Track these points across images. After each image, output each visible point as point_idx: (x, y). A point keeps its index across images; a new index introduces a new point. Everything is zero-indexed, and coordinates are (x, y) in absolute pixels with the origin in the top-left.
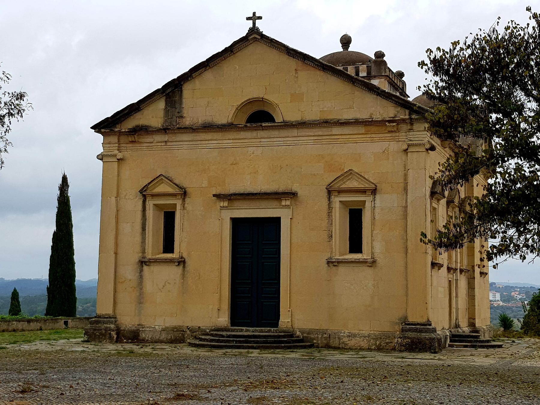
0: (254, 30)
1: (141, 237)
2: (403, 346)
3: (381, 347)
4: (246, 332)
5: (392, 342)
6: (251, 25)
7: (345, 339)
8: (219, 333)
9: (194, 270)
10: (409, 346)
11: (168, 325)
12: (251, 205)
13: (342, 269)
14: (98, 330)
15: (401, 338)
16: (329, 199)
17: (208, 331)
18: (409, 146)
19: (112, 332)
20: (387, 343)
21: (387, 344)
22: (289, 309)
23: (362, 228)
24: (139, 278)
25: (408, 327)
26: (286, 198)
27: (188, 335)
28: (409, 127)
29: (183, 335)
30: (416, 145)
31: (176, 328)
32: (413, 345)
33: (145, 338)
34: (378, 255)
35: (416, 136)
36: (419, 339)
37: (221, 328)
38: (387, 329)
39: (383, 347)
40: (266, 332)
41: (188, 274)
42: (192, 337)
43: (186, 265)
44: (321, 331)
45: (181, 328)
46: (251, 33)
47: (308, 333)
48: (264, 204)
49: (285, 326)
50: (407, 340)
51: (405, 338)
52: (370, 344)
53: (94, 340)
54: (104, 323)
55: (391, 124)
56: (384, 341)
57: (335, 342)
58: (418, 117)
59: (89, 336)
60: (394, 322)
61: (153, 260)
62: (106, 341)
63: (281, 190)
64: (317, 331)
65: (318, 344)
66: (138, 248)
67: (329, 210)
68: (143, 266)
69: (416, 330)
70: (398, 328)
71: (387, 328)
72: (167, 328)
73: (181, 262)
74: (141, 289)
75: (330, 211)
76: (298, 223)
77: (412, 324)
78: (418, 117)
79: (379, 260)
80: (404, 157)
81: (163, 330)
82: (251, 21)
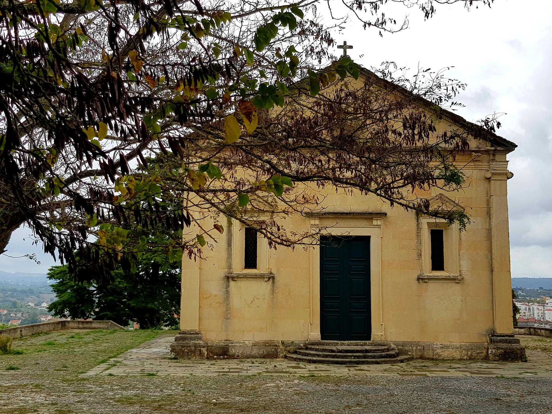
0: (345, 58)
1: (227, 253)
2: (497, 356)
3: (473, 357)
4: (341, 345)
5: (482, 353)
6: (342, 54)
7: (439, 351)
11: (257, 340)
13: (432, 285)
14: (187, 347)
15: (494, 349)
16: (418, 219)
17: (302, 345)
18: (493, 174)
19: (202, 349)
20: (478, 354)
21: (478, 355)
22: (381, 324)
23: (256, 257)
24: (226, 294)
25: (499, 338)
26: (378, 219)
27: (281, 349)
28: (491, 158)
29: (276, 350)
30: (499, 174)
31: (268, 343)
35: (498, 166)
38: (475, 340)
39: (474, 357)
40: (362, 345)
43: (276, 281)
44: (414, 343)
45: (273, 343)
47: (402, 346)
48: (353, 223)
50: (501, 351)
51: (498, 348)
53: (182, 357)
54: (191, 339)
57: (429, 354)
58: (502, 149)
60: (481, 334)
62: (196, 358)
63: (370, 211)
64: (411, 344)
66: (224, 264)
68: (229, 282)
69: (506, 341)
71: (475, 339)
72: (258, 342)
73: (271, 278)
74: (228, 305)
77: (501, 336)
78: (502, 149)
79: (466, 277)
80: (486, 184)
81: (254, 345)
82: (347, 50)
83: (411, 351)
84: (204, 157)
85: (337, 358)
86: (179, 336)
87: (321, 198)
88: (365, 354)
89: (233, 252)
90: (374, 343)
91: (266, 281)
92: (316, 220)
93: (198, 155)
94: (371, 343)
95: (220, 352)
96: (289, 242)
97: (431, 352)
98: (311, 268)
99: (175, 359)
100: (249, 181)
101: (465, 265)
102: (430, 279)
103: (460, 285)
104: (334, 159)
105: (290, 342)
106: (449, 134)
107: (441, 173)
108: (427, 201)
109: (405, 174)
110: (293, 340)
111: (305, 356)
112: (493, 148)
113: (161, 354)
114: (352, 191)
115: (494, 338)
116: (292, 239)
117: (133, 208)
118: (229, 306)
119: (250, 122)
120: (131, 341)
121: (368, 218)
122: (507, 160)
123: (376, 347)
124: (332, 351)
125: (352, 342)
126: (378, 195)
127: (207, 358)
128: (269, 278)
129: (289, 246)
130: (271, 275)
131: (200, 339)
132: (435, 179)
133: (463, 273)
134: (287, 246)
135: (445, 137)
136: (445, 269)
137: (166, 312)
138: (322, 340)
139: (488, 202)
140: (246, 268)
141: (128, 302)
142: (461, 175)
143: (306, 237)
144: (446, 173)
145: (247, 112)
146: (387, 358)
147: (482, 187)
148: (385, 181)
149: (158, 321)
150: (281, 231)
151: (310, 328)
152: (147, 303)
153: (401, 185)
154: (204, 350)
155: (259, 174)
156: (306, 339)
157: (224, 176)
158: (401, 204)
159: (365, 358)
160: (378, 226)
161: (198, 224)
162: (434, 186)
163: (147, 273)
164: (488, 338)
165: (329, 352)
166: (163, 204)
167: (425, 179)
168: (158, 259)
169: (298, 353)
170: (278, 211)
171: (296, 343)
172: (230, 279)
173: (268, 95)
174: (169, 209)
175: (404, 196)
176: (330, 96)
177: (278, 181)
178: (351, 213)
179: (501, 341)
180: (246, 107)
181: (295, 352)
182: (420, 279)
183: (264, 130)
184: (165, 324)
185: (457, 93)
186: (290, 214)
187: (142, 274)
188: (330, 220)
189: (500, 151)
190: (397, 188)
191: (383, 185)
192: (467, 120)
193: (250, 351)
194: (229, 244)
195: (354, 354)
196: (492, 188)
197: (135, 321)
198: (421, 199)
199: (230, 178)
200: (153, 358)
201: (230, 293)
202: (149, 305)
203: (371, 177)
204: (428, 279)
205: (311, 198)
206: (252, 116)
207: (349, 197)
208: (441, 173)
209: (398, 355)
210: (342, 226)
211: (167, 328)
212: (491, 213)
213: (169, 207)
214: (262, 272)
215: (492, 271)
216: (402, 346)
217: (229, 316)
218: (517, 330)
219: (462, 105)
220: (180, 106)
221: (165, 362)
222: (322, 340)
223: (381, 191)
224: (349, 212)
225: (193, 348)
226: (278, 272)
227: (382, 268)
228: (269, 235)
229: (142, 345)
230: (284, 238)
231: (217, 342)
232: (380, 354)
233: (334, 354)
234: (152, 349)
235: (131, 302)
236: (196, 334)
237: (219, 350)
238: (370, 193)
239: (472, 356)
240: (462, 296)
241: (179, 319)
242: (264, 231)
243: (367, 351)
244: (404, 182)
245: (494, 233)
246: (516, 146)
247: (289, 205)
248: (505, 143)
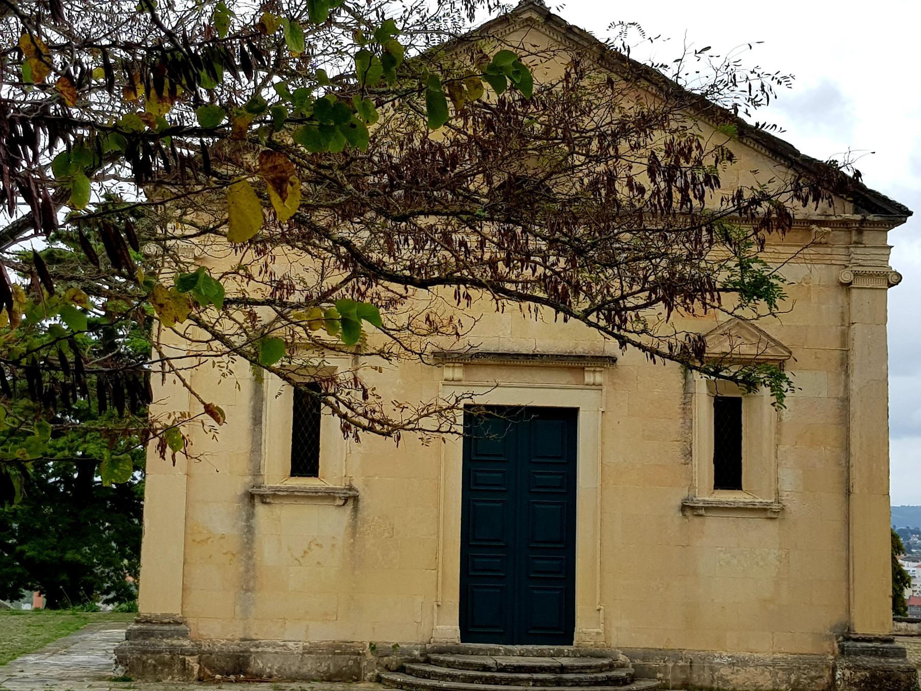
1: (250, 439)
4: (506, 655)
5: (821, 677)
7: (725, 671)
8: (441, 658)
9: (379, 517)
10: (866, 686)
11: (315, 639)
12: (512, 379)
13: (713, 523)
14: (154, 653)
15: (849, 668)
16: (685, 378)
17: (416, 653)
18: (856, 274)
19: (187, 658)
20: (812, 679)
21: (812, 681)
23: (317, 449)
25: (859, 645)
26: (598, 369)
27: (369, 662)
28: (854, 238)
30: (870, 275)
31: (339, 647)
32: (874, 683)
33: (263, 670)
34: (787, 496)
36: (885, 671)
37: (447, 647)
38: (807, 648)
39: (804, 686)
40: (552, 656)
41: (366, 526)
42: (379, 668)
43: (361, 505)
44: (670, 653)
45: (350, 647)
46: (522, 10)
48: (540, 377)
49: (593, 643)
50: (863, 673)
51: (858, 668)
52: (778, 680)
53: (141, 676)
54: (163, 635)
55: (823, 229)
56: (805, 674)
59: (128, 668)
60: (820, 634)
61: (285, 493)
62: (173, 678)
63: (580, 351)
64: (663, 654)
65: (666, 680)
66: (243, 464)
67: (685, 399)
68: (253, 506)
69: (875, 652)
70: (830, 648)
71: (807, 647)
72: (317, 646)
74: (250, 558)
75: (686, 401)
76: (619, 422)
77: (864, 640)
80: (841, 298)
81: (309, 651)
83: (663, 669)
84: (201, 223)
85: (496, 684)
86: (136, 627)
87: (467, 323)
88: (559, 676)
89: (266, 436)
90: (580, 651)
91: (339, 506)
92: (456, 370)
93: (188, 218)
94: (573, 652)
95: (231, 664)
96: (389, 425)
97: (706, 675)
98: (442, 478)
99: (124, 679)
100: (303, 280)
101: (789, 480)
102: (711, 508)
103: (777, 523)
104: (495, 240)
105: (391, 646)
106: (747, 195)
107: (732, 279)
108: (701, 338)
109: (652, 278)
110: (395, 641)
111: (424, 677)
112: (858, 217)
113: (93, 668)
114: (536, 310)
115: (850, 643)
116: (396, 417)
117: (24, 362)
118: (251, 562)
119: (284, 201)
120: (25, 636)
121: (573, 368)
122: (889, 243)
123: (585, 659)
124: (486, 668)
125: (530, 647)
126: (590, 324)
127: (200, 680)
128: (346, 500)
129: (388, 434)
130: (351, 493)
131: (184, 635)
132: (719, 290)
133: (784, 496)
134: (383, 434)
135: (738, 201)
136: (743, 488)
137: (107, 570)
138: (462, 642)
139: (845, 339)
140: (293, 474)
141: (18, 548)
142: (774, 281)
143: (426, 416)
144: (742, 276)
145: (278, 178)
146: (607, 685)
147: (832, 303)
148: (608, 291)
149: (90, 590)
150: (371, 399)
151: (435, 615)
152: (64, 551)
153: (642, 302)
154: (192, 661)
155: (326, 264)
156: (426, 639)
157: (246, 270)
158: (639, 346)
159: (559, 686)
160: (598, 386)
161: (183, 381)
162: (714, 308)
163: (68, 480)
164: (836, 645)
165: (478, 670)
166: (106, 322)
167: (695, 290)
168: (92, 448)
169: (408, 671)
170: (369, 352)
171: (403, 649)
172: (257, 501)
173: (332, 124)
174: (121, 333)
175: (650, 326)
176: (488, 97)
177: (350, 312)
178: (536, 355)
179: (863, 652)
180: (275, 167)
181: (401, 669)
182: (686, 508)
183: (338, 172)
184: (105, 597)
185: (771, 97)
186: (394, 359)
187: (55, 482)
188: (489, 370)
189: (873, 222)
190: (632, 309)
191: (604, 302)
192: (802, 152)
193: (297, 664)
194: (257, 419)
195: (535, 676)
196: (853, 305)
197: (36, 590)
198: (687, 335)
199: (260, 273)
200: (75, 678)
201: (256, 532)
202: (69, 556)
203: (578, 282)
204: (706, 509)
205: (445, 322)
206: (289, 186)
207: (530, 319)
208: (732, 279)
209: (633, 678)
210: (516, 385)
211: (110, 607)
212: (851, 363)
213: (121, 328)
214: (331, 486)
215: (848, 493)
216: (644, 659)
217: (251, 584)
218: (903, 625)
219: (778, 128)
220: (137, 142)
221: (101, 686)
222: (462, 642)
223: (597, 316)
224: (531, 353)
225: (167, 656)
226: (367, 485)
227: (602, 481)
228: (343, 409)
229: (50, 646)
230: (377, 416)
231: (223, 642)
232: (592, 676)
233: (488, 674)
234: (73, 656)
235: (25, 547)
236: (176, 625)
237: (228, 662)
238: (572, 320)
239: (799, 683)
240: (780, 548)
241: (137, 587)
242: (332, 399)
243: (563, 669)
244: (650, 297)
245: (856, 407)
246: (910, 214)
247: (395, 339)
248: (885, 207)
